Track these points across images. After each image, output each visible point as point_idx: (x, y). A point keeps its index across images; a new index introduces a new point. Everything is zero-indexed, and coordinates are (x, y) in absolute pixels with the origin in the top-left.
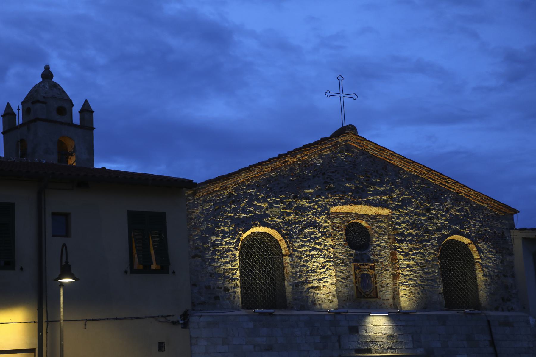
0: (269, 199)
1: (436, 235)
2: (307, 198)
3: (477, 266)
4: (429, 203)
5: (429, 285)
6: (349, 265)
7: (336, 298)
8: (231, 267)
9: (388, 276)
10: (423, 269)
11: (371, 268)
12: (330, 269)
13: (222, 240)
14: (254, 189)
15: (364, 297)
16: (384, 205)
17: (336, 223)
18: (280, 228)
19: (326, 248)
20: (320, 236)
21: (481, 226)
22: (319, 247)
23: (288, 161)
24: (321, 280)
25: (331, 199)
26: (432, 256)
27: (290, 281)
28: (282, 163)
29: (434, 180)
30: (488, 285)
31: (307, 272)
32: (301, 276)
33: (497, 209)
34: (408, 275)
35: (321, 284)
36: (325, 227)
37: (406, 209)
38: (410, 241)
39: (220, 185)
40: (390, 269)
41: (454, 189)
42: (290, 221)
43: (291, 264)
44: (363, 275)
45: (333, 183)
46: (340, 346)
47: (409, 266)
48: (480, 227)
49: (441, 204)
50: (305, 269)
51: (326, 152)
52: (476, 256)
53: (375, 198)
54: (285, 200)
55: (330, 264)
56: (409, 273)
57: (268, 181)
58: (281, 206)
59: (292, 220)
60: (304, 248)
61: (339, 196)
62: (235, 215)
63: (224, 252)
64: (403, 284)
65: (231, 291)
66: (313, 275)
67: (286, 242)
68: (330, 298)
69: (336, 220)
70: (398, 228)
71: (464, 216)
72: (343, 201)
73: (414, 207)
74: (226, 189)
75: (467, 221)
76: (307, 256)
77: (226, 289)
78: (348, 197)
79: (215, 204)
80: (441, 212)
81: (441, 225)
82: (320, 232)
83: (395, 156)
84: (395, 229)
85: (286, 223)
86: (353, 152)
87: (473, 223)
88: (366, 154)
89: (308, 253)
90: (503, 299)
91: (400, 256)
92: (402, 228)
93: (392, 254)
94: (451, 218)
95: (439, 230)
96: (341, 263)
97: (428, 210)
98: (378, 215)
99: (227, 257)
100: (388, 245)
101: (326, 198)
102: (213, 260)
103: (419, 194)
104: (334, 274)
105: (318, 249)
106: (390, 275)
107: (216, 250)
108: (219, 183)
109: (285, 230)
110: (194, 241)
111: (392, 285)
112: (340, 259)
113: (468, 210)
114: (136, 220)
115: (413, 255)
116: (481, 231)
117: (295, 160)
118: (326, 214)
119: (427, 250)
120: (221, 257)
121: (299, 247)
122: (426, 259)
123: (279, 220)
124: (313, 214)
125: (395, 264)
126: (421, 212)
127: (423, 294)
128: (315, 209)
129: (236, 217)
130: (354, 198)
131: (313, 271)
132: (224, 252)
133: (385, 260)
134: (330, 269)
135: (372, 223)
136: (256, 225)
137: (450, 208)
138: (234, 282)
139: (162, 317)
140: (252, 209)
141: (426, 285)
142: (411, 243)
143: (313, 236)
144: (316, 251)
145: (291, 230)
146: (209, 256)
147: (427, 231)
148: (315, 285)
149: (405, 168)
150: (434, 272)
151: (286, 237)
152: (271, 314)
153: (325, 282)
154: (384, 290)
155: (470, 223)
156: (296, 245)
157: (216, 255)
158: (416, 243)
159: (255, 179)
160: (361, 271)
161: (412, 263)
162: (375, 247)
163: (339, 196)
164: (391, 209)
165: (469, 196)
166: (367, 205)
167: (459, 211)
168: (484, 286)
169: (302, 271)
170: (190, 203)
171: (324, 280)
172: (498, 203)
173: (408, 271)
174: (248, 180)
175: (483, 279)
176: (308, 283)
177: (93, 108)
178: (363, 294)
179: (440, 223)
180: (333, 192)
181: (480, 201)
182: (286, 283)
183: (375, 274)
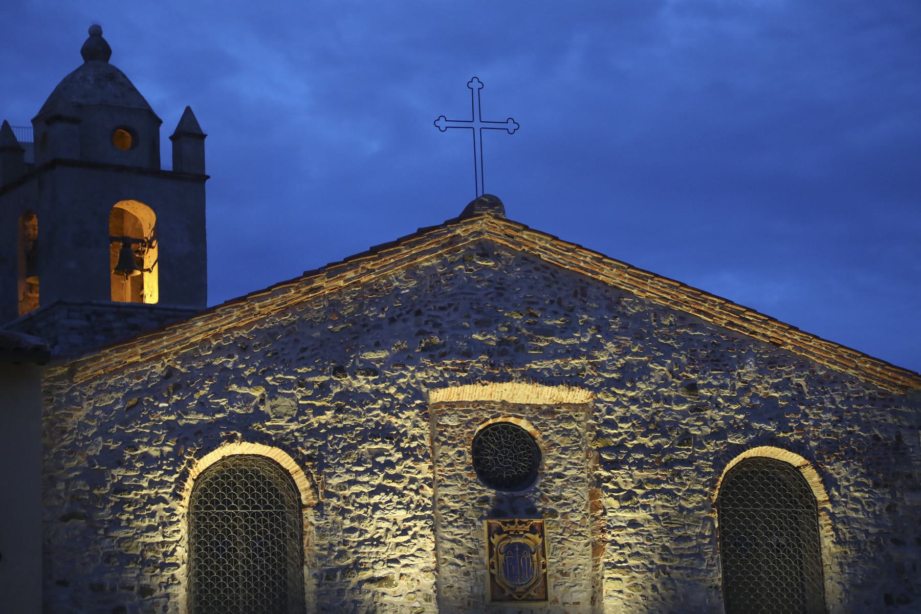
0: (269, 379)
1: (710, 447)
2: (370, 369)
3: (824, 520)
4: (694, 371)
5: (685, 568)
6: (478, 523)
7: (433, 603)
8: (161, 539)
9: (580, 548)
10: (672, 529)
11: (533, 530)
12: (422, 536)
13: (140, 477)
14: (231, 356)
15: (511, 599)
16: (574, 380)
17: (447, 426)
18: (296, 443)
19: (414, 487)
20: (399, 460)
21: (838, 421)
22: (394, 485)
23: (321, 287)
24: (396, 561)
25: (431, 373)
26: (698, 498)
27: (314, 565)
28: (306, 293)
29: (711, 316)
30: (849, 565)
31: (360, 544)
32: (342, 554)
33: (884, 381)
34: (629, 545)
35: (396, 570)
36: (414, 438)
37: (633, 389)
38: (640, 465)
39: (140, 352)
40: (587, 531)
41: (764, 335)
42: (321, 426)
43: (318, 528)
44: (511, 547)
45: (441, 334)
47: (633, 523)
48: (835, 426)
49: (728, 374)
50: (354, 537)
51: (427, 260)
52: (820, 495)
53: (549, 364)
54: (311, 379)
55: (421, 523)
56: (632, 540)
57: (270, 335)
58: (298, 393)
59: (327, 423)
60: (356, 489)
61: (452, 364)
62: (180, 417)
63: (146, 504)
64: (614, 567)
65: (158, 593)
66: (374, 550)
67: (308, 475)
68: (417, 604)
69: (446, 420)
70: (609, 435)
71: (793, 398)
72: (464, 375)
73: (656, 383)
74: (158, 358)
75: (797, 411)
76: (362, 506)
77: (146, 591)
78: (476, 364)
79: (126, 397)
80: (727, 393)
81: (727, 423)
82: (399, 449)
83: (604, 263)
84: (600, 435)
85: (312, 432)
86: (497, 258)
87: (815, 414)
88: (533, 262)
89: (364, 500)
90: (888, 599)
91: (611, 500)
92: (620, 434)
93: (593, 496)
94: (754, 407)
95: (719, 434)
96: (456, 521)
97: (692, 387)
98: (560, 405)
99: (153, 515)
100: (582, 475)
101: (420, 370)
102: (116, 524)
103: (668, 351)
104: (430, 546)
105: (393, 490)
106: (587, 545)
107: (124, 501)
108: (134, 346)
109: (308, 449)
110: (68, 482)
111: (589, 570)
112: (454, 512)
113: (804, 384)
115: (645, 496)
116: (836, 435)
117: (341, 283)
118: (418, 406)
119: (683, 484)
120: (137, 517)
121: (341, 487)
122: (680, 506)
123: (293, 426)
124: (384, 409)
125: (597, 518)
126: (673, 393)
127: (667, 590)
128: (390, 395)
129: (182, 423)
130: (493, 366)
131: (377, 542)
132: (146, 504)
133: (573, 511)
134: (422, 536)
135: (544, 424)
136: (231, 439)
137: (754, 381)
138: (167, 573)
140: (223, 402)
141: (677, 568)
142: (640, 469)
143: (381, 459)
144: (387, 494)
145: (323, 448)
146: (106, 514)
147: (686, 438)
148: (378, 574)
149: (635, 291)
150: (704, 537)
151: (309, 464)
153: (406, 565)
154: (569, 581)
155: (805, 416)
156: (335, 481)
157: (123, 512)
158: (656, 468)
159: (236, 334)
160: (505, 539)
161: (641, 515)
162: (551, 481)
163: (452, 364)
164: (590, 388)
165: (807, 352)
166: (528, 382)
167: (776, 387)
168: (837, 569)
169: (345, 543)
170: (60, 395)
171: (403, 562)
172: (882, 367)
173: (630, 535)
174: (216, 336)
175: (834, 550)
176: (359, 570)
177: (204, 126)
178: (508, 592)
179: (723, 418)
180: (436, 354)
181: (835, 363)
182: (306, 570)
183: (543, 544)
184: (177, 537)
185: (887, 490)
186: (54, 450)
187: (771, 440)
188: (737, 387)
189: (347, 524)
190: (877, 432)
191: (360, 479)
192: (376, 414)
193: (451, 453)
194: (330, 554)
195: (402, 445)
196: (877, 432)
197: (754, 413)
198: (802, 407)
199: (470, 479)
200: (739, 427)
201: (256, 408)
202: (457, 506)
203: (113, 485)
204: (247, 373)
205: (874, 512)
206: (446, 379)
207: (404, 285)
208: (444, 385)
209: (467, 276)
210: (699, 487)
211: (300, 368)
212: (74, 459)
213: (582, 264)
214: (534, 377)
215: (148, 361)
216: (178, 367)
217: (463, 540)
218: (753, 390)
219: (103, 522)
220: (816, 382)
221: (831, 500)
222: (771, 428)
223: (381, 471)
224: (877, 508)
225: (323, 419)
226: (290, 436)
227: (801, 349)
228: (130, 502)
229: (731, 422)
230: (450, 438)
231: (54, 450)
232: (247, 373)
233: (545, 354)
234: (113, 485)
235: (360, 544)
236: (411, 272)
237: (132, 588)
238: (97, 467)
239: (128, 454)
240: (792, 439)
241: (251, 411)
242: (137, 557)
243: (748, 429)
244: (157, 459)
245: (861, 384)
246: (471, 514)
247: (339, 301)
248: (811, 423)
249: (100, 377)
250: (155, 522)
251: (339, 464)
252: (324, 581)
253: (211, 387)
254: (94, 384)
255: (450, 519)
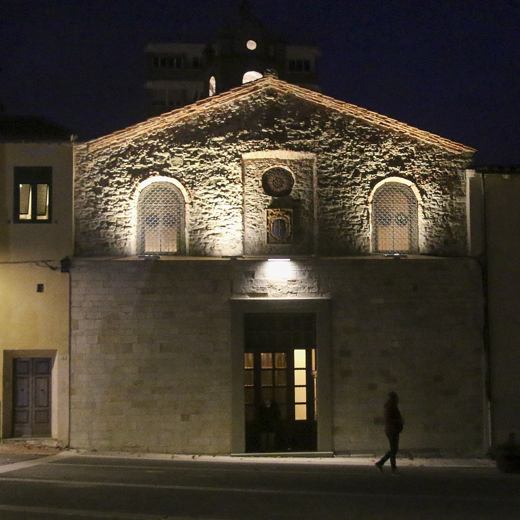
0: (171, 149)
2: (215, 144)
3: (420, 209)
8: (125, 216)
16: (306, 149)
18: (182, 177)
19: (234, 195)
21: (428, 166)
25: (243, 146)
30: (429, 228)
31: (209, 219)
33: (450, 148)
36: (235, 174)
37: (335, 152)
41: (396, 128)
42: (194, 169)
50: (206, 217)
51: (244, 97)
54: (189, 149)
58: (184, 155)
59: (196, 168)
60: (208, 196)
61: (253, 142)
65: (122, 238)
68: (233, 245)
72: (258, 147)
75: (410, 161)
76: (210, 203)
77: (117, 237)
80: (377, 154)
82: (228, 179)
85: (190, 172)
86: (275, 96)
89: (211, 201)
95: (374, 172)
98: (303, 160)
101: (238, 145)
105: (224, 196)
112: (253, 206)
113: (414, 150)
117: (204, 108)
118: (236, 161)
123: (182, 169)
124: (222, 162)
129: (134, 168)
138: (127, 230)
140: (152, 159)
145: (194, 179)
146: (102, 206)
151: (187, 185)
155: (413, 164)
156: (198, 193)
157: (108, 205)
163: (253, 142)
165: (416, 135)
167: (401, 151)
170: (83, 157)
174: (150, 132)
181: (429, 140)
184: (130, 215)
185: (449, 196)
186: (81, 179)
187: (396, 174)
188: (383, 151)
189: (204, 211)
190: (446, 171)
191: (209, 192)
192: (218, 164)
193: (252, 181)
194: (195, 223)
195: (229, 177)
196: (446, 171)
197: (391, 163)
198: (412, 160)
199: (260, 192)
200: (383, 169)
201: (166, 162)
202: (254, 204)
203: (105, 194)
204: (162, 147)
205: (442, 206)
206: (249, 149)
207: (233, 109)
208: (248, 151)
209: (261, 104)
210: (362, 195)
211: (185, 144)
212: (89, 183)
213: (314, 98)
214: (291, 148)
215: (120, 142)
216: (133, 145)
217: (256, 218)
218: (390, 152)
219: (100, 209)
220: (419, 149)
221: (423, 200)
222: (397, 169)
223: (219, 188)
224: (444, 204)
225: (194, 166)
226: (180, 174)
227: (413, 135)
228: (111, 201)
229: (379, 166)
230: (252, 174)
231: (81, 179)
232: (162, 147)
233: (295, 137)
234: (105, 194)
235: (209, 219)
236: (237, 103)
237: (112, 236)
238: (98, 186)
239: (111, 181)
240: (407, 174)
241: (163, 163)
242: (115, 223)
243: (387, 170)
244: (123, 183)
245: (441, 149)
246: (260, 207)
247: (204, 116)
248: (416, 167)
249: (100, 149)
250: (121, 209)
251: (200, 185)
252: (193, 234)
253: (147, 153)
254: (98, 152)
255: (251, 209)
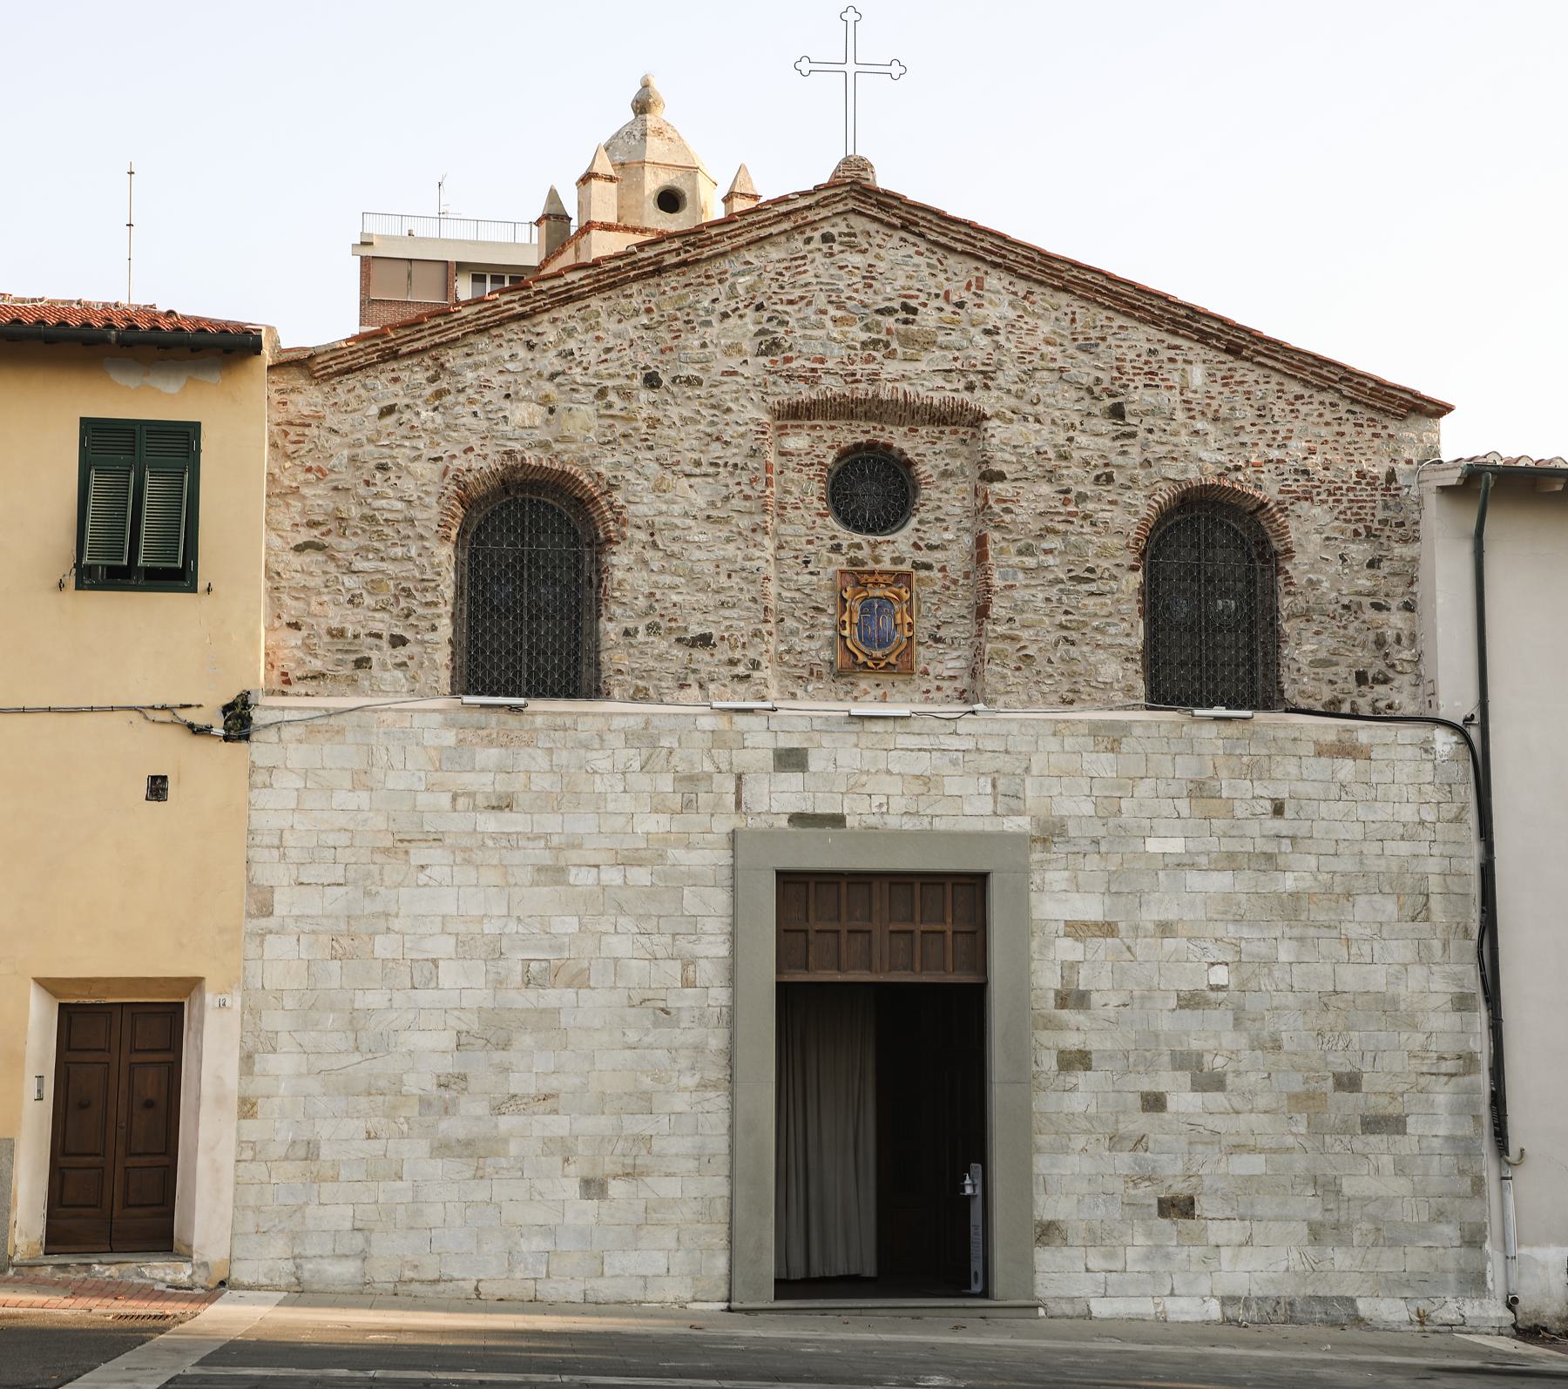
46: (738, 804)
114: (101, 440)
139: (164, 708)
152: (517, 709)
